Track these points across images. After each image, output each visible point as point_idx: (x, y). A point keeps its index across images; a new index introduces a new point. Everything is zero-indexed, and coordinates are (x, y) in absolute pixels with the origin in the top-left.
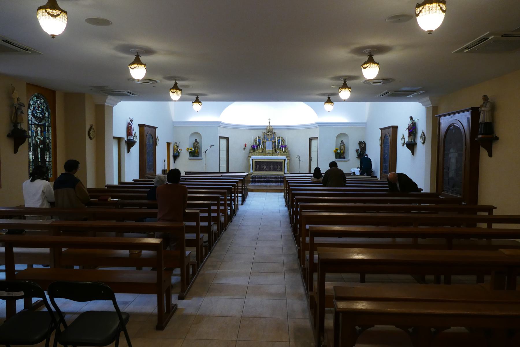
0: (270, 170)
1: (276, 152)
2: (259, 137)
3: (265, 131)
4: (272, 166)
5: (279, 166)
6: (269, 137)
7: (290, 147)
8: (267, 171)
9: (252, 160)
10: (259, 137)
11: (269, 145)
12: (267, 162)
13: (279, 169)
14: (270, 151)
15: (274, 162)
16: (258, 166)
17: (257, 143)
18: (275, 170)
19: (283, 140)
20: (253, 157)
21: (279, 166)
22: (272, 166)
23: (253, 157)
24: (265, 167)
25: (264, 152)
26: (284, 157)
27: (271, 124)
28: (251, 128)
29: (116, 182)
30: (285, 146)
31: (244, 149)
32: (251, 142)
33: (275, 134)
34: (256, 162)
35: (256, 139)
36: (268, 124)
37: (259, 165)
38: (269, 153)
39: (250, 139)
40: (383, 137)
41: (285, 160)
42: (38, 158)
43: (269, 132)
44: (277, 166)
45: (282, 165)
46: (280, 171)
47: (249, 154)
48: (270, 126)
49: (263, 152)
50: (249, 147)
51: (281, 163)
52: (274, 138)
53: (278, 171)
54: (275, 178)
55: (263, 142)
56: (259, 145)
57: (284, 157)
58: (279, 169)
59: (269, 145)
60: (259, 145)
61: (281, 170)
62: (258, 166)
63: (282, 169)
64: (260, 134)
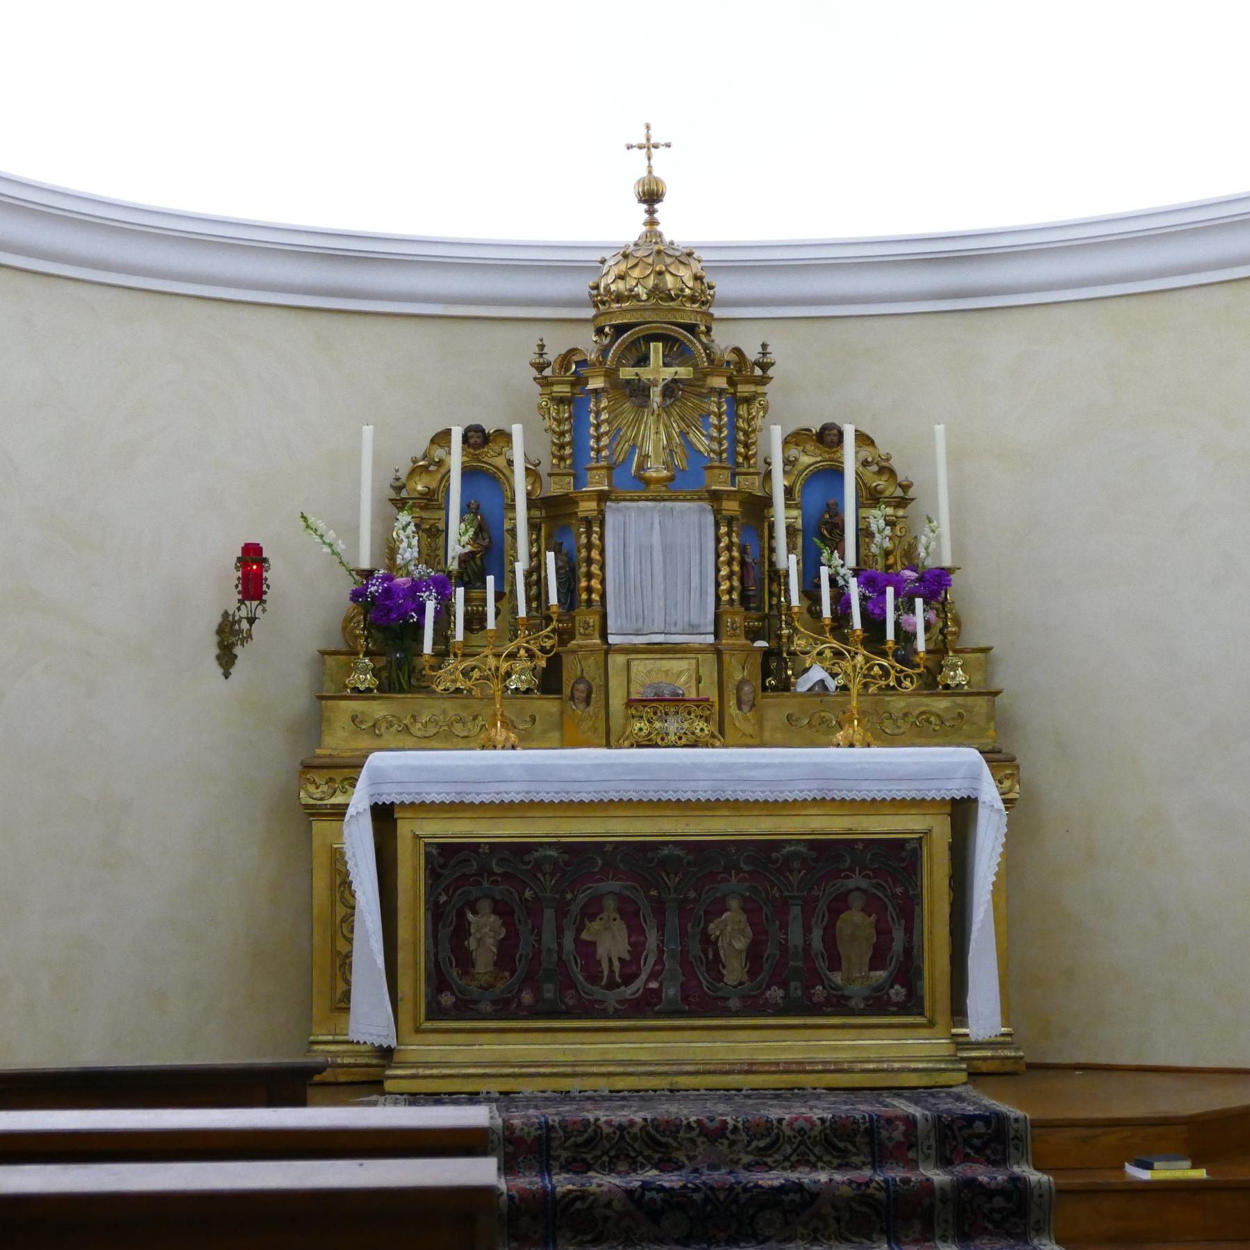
0: (701, 1002)
1: (775, 670)
2: (477, 438)
3: (587, 342)
4: (732, 933)
5: (856, 924)
6: (653, 440)
7: (992, 603)
8: (644, 1007)
9: (384, 816)
10: (477, 438)
11: (661, 570)
12: (640, 858)
13: (858, 976)
14: (678, 674)
15: (765, 852)
16: (485, 930)
17: (458, 540)
18: (796, 987)
19: (889, 490)
20: (400, 768)
21: (856, 924)
22: (732, 933)
23: (400, 768)
24: (611, 942)
25: (563, 683)
26: (953, 765)
27: (678, 225)
28: (338, 288)
29: (396, 816)
30: (935, 584)
31: (229, 640)
32: (337, 530)
33: (746, 377)
34: (447, 861)
35: (429, 465)
36: (627, 226)
37: (505, 922)
38: (662, 702)
39: (324, 472)
40: (749, 741)
41: (962, 812)
42: (546, 1198)
43: (654, 342)
44: (845, 911)
45: (909, 908)
46: (877, 1005)
47: (316, 723)
48: (654, 250)
49: (550, 680)
50: (308, 601)
51: (898, 858)
52: (740, 449)
53: (838, 1004)
54: (838, 1141)
55: (553, 514)
56: (487, 556)
57: (953, 765)
58: (858, 976)
59: (661, 570)
60: (487, 556)
61: (901, 989)
62: (485, 930)
63: (910, 972)
64: (496, 386)
